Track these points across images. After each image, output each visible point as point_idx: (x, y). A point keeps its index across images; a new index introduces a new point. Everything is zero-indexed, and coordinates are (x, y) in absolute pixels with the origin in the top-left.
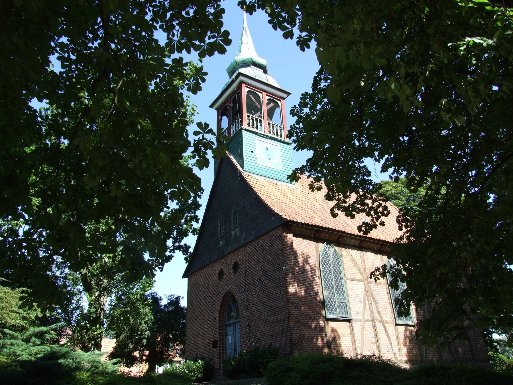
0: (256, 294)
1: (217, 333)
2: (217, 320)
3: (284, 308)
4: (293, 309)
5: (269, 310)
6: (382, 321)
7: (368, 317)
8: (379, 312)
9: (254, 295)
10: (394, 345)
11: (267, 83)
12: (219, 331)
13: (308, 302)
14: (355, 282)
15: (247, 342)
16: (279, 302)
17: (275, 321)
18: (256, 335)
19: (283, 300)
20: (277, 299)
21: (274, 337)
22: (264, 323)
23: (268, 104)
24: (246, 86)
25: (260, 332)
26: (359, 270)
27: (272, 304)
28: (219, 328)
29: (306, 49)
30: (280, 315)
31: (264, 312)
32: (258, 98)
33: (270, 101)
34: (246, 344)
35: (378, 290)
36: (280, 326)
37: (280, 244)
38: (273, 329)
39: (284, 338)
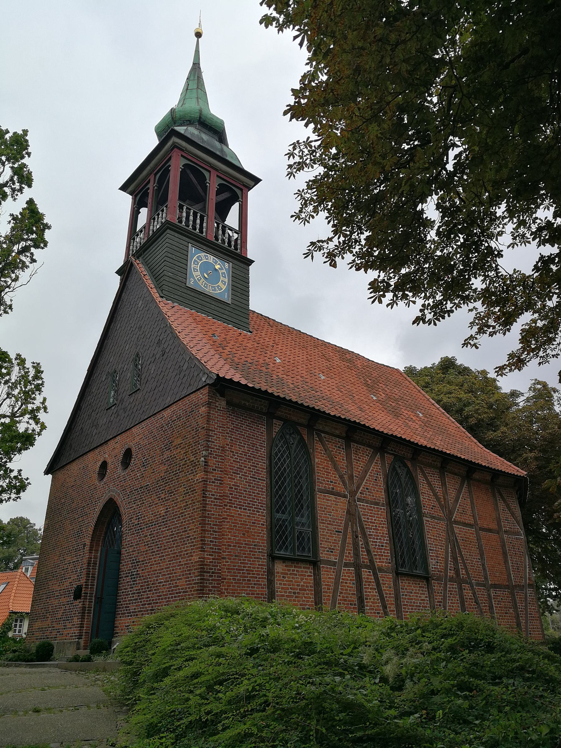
0: (152, 505)
1: (84, 572)
2: (87, 548)
3: (195, 532)
4: (211, 534)
5: (170, 535)
6: (372, 566)
7: (349, 557)
8: (369, 552)
9: (149, 506)
10: (390, 611)
11: (221, 156)
12: (87, 568)
13: (241, 524)
14: (333, 497)
15: (128, 592)
16: (189, 520)
17: (177, 556)
18: (144, 579)
19: (195, 519)
20: (185, 515)
21: (173, 584)
22: (160, 557)
23: (218, 193)
24: (182, 156)
25: (152, 574)
26: (341, 477)
27: (176, 524)
28: (88, 563)
29: (263, 24)
30: (186, 544)
31: (161, 538)
32: (202, 179)
33: (222, 189)
34: (127, 595)
35: (371, 513)
36: (185, 564)
37: (202, 418)
38: (173, 570)
39: (189, 588)
